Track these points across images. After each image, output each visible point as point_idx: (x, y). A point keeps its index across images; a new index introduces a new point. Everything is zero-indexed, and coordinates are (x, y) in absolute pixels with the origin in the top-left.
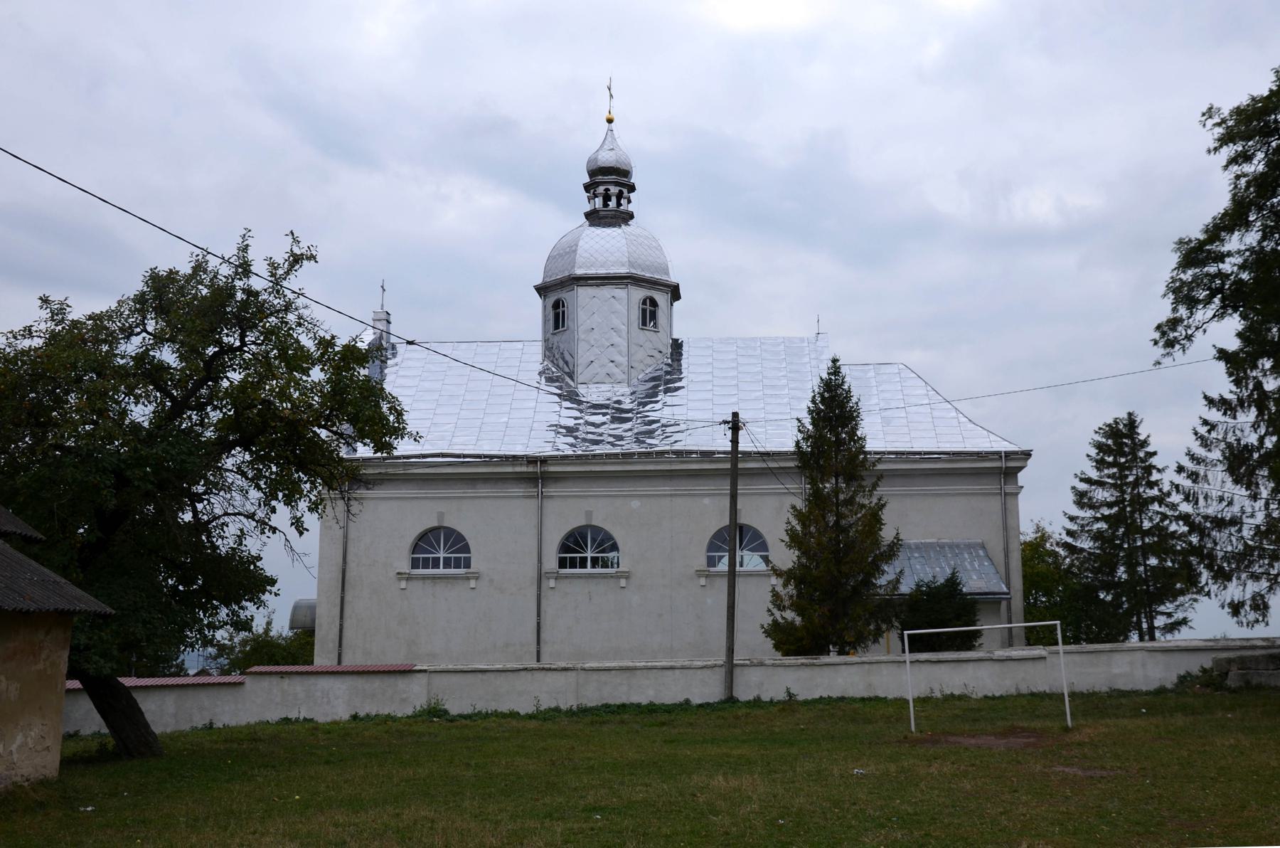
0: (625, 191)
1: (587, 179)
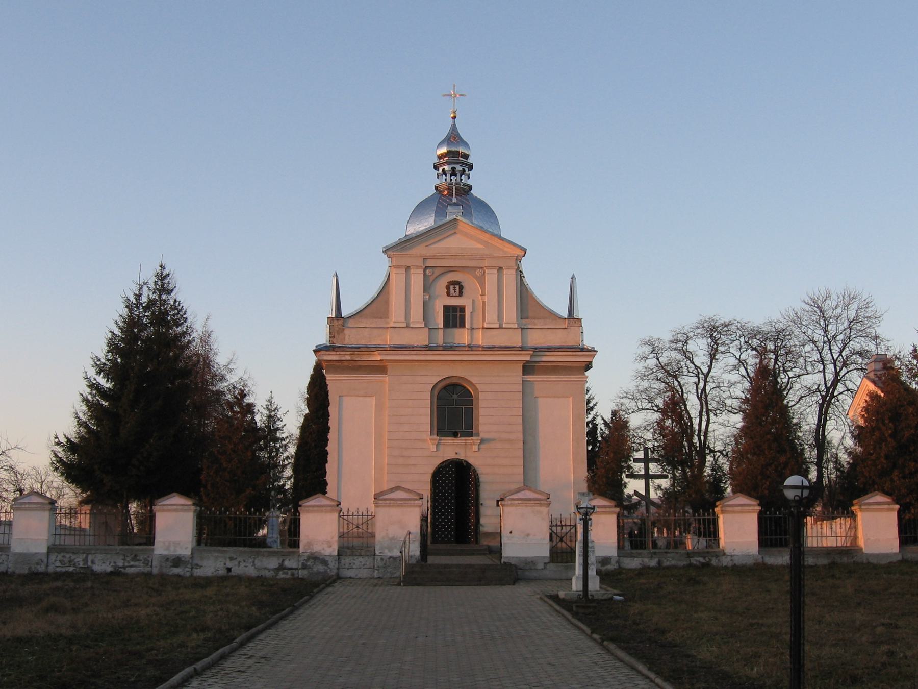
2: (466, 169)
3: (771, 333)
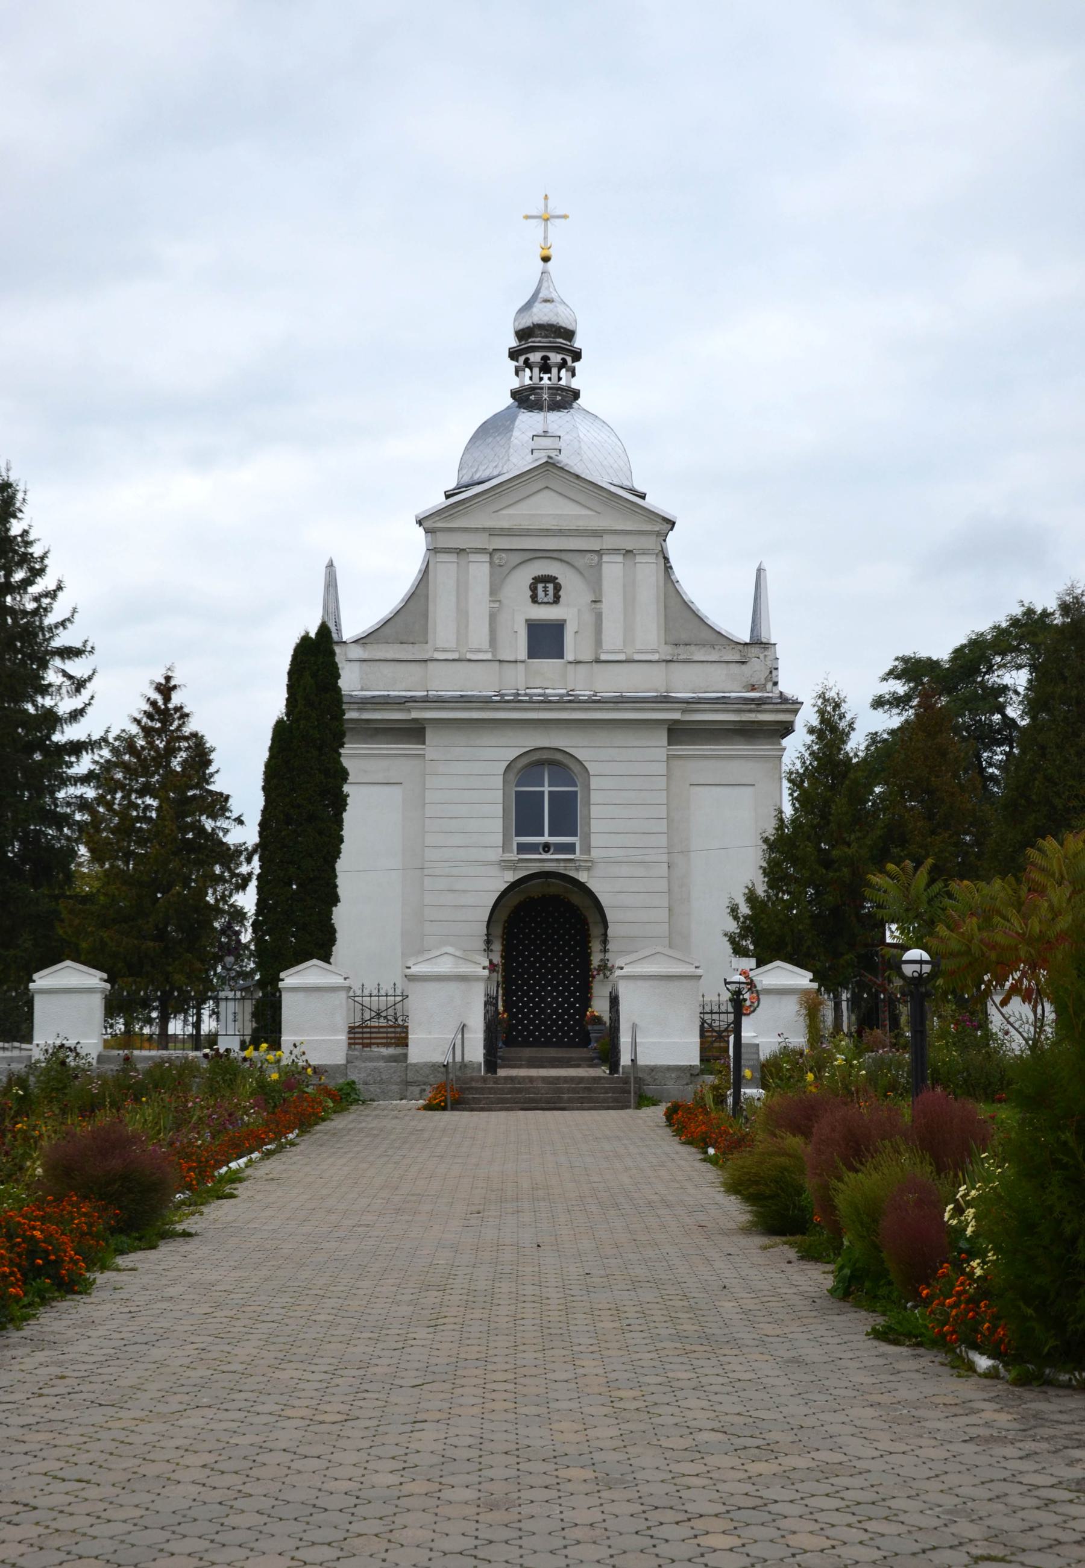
0: (569, 359)
1: (513, 342)
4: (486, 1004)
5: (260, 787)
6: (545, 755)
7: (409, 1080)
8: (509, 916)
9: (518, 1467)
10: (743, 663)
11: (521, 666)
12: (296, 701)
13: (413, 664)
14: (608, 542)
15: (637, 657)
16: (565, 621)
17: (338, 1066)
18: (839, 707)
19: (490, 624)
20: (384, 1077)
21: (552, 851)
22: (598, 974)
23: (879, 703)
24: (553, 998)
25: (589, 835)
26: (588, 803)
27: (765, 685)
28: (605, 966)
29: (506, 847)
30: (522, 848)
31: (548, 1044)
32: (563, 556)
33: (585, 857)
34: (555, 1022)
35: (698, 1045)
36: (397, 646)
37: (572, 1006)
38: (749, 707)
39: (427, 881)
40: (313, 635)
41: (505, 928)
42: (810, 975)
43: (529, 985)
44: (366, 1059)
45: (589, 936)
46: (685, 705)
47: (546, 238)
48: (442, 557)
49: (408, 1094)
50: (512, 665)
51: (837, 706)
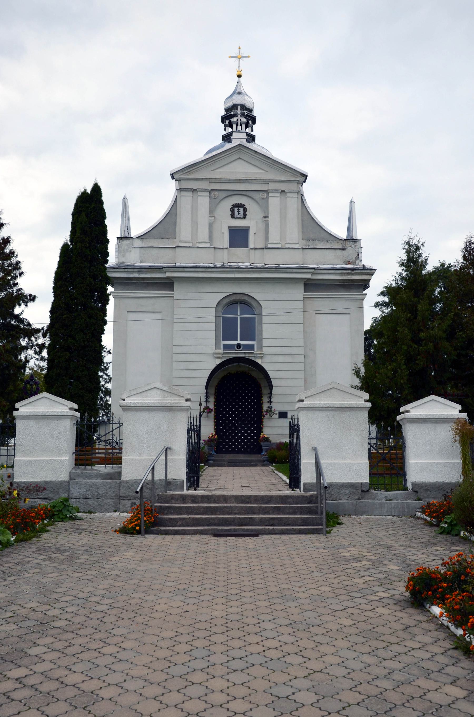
2: (250, 122)
3: (63, 557)
4: (189, 431)
5: (52, 288)
6: (238, 297)
7: (121, 495)
8: (218, 383)
9: (227, 610)
10: (344, 249)
11: (225, 251)
12: (76, 231)
13: (168, 249)
14: (272, 186)
15: (287, 246)
16: (249, 227)
17: (61, 483)
18: (419, 249)
19: (209, 229)
20: (101, 492)
21: (241, 349)
22: (267, 414)
23: (377, 305)
24: (242, 427)
25: (262, 340)
26: (261, 323)
27: (355, 261)
28: (271, 410)
29: (217, 346)
30: (225, 347)
31: (239, 452)
32: (248, 193)
33: (260, 352)
34: (243, 441)
35: (368, 465)
36: (160, 240)
37: (252, 432)
38: (347, 271)
39: (175, 365)
40: (89, 191)
41: (216, 389)
42: (459, 407)
43: (229, 420)
44: (87, 477)
45: (262, 394)
46: (313, 270)
47: (239, 67)
48: (184, 193)
49: (121, 507)
50: (221, 250)
51: (418, 248)
